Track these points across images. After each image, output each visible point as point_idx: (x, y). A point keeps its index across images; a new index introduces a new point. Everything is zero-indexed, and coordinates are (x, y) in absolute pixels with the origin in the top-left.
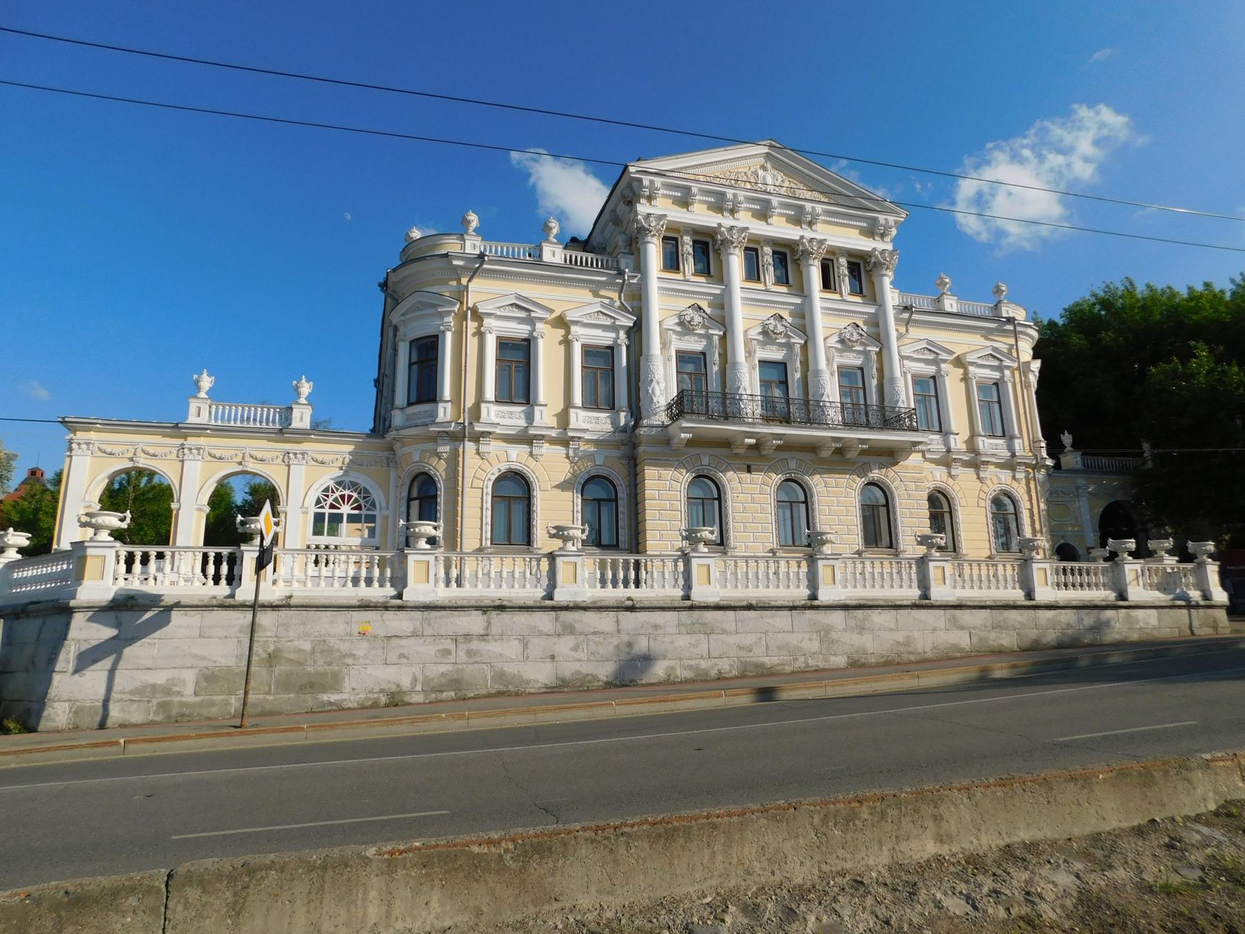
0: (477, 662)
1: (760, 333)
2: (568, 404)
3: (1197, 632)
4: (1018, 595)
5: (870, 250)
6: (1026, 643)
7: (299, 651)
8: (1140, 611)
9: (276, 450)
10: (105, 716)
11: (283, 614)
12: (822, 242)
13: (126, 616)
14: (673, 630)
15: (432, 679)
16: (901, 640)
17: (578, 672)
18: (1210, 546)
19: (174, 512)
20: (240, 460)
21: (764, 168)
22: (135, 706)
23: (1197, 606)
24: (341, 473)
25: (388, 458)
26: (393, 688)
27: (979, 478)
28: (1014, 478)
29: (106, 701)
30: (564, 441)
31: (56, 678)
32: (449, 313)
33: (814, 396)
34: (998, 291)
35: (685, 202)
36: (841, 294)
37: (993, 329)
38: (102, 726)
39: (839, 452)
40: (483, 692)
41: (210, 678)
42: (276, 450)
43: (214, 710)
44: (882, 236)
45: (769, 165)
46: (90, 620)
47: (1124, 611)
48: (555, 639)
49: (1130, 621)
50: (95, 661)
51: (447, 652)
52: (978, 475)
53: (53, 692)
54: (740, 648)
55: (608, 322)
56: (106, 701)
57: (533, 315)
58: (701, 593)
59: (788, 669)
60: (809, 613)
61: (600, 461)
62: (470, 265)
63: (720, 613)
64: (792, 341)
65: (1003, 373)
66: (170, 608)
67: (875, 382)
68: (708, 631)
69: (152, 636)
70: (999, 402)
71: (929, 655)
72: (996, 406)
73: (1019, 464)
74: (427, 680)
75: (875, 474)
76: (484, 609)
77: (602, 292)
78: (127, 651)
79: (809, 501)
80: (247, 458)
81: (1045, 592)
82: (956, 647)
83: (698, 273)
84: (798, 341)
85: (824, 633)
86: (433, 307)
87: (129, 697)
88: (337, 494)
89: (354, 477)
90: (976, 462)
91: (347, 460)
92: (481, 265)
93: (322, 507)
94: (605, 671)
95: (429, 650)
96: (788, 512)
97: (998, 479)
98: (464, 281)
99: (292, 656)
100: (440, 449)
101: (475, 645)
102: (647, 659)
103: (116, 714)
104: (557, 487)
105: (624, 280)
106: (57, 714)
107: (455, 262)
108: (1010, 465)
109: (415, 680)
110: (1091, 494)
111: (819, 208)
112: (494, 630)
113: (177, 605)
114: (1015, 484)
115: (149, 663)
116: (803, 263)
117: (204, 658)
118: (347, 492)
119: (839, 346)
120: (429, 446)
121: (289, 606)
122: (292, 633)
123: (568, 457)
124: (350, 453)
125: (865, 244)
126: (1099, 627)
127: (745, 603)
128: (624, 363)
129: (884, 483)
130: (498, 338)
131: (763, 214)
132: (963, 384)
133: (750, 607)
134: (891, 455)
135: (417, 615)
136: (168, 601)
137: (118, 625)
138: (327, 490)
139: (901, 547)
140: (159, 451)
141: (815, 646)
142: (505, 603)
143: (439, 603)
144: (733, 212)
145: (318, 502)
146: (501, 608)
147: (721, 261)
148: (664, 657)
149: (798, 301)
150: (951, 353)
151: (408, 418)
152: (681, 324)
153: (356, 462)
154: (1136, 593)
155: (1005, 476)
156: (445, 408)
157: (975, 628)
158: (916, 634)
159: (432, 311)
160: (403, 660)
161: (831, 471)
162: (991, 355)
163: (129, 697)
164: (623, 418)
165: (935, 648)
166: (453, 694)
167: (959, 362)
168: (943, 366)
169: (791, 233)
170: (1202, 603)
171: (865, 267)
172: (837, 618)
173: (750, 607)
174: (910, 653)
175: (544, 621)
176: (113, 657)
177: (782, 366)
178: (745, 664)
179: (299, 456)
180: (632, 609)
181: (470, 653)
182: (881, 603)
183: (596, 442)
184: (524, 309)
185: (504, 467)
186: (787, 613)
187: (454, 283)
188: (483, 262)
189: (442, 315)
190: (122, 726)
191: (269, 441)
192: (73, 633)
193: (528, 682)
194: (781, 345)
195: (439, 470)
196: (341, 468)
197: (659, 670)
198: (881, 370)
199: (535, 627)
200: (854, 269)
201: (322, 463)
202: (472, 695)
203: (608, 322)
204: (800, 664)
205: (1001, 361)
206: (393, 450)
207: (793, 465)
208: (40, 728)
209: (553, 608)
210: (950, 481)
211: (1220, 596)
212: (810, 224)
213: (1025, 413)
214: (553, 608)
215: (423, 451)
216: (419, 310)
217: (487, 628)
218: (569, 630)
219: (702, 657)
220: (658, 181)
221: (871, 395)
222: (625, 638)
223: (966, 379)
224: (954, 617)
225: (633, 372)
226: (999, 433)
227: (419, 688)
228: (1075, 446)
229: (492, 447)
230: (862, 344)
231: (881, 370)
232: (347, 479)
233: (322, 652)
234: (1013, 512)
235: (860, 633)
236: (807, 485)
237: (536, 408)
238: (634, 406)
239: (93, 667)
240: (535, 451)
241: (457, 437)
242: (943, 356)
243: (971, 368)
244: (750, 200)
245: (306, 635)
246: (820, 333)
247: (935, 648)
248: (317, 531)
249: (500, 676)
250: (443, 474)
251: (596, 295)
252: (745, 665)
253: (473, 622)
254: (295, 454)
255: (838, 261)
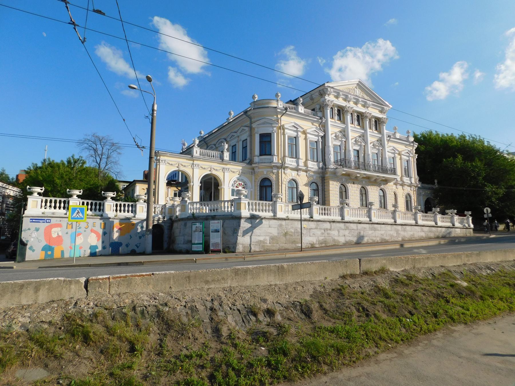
0: (329, 236)
1: (354, 141)
2: (284, 156)
3: (467, 235)
4: (413, 222)
5: (364, 112)
6: (436, 237)
7: (292, 232)
8: (457, 229)
9: (219, 167)
10: (251, 249)
11: (287, 221)
12: (370, 114)
13: (253, 220)
14: (368, 229)
15: (320, 241)
16: (412, 234)
17: (350, 240)
18: (470, 213)
19: (191, 186)
20: (177, 166)
21: (357, 88)
22: (257, 246)
23: (468, 228)
24: (239, 176)
25: (252, 172)
26: (312, 243)
27: (403, 189)
28: (411, 189)
29: (250, 245)
30: (306, 171)
31: (239, 237)
32: (275, 127)
33: (367, 162)
34: (395, 129)
35: (337, 97)
36: (373, 130)
37: (315, 120)
38: (250, 252)
39: (376, 180)
40: (330, 244)
41: (272, 238)
42: (219, 167)
43: (274, 248)
44: (384, 113)
45: (357, 87)
46: (245, 221)
47: (454, 229)
48: (345, 231)
49: (455, 231)
50: (247, 233)
51: (323, 234)
52: (403, 188)
53: (238, 241)
54: (381, 234)
55: (317, 134)
56: (250, 245)
57: (298, 130)
58: (347, 218)
59: (390, 241)
60: (395, 226)
61: (315, 177)
62: (282, 111)
63: (377, 225)
64: (362, 144)
65: (409, 158)
66: (262, 219)
67: (343, 151)
68: (375, 230)
69: (259, 226)
70: (317, 149)
71: (417, 238)
72: (294, 146)
73: (413, 185)
74: (319, 241)
75: (382, 187)
76: (330, 222)
77: (314, 124)
78: (254, 230)
79: (367, 193)
80: (180, 166)
81: (440, 224)
82: (422, 237)
83: (338, 120)
84: (363, 144)
85: (397, 231)
86: (270, 124)
87: (255, 244)
88: (238, 183)
89: (242, 178)
90: (403, 185)
91: (240, 172)
92: (286, 112)
93: (234, 187)
94: (355, 239)
95: (318, 232)
96: (291, 191)
97: (407, 189)
98: (279, 116)
99: (290, 233)
100: (274, 171)
101: (329, 232)
102: (363, 237)
103: (253, 248)
104: (304, 185)
105: (322, 121)
106: (240, 248)
107: (278, 110)
108: (410, 186)
109: (317, 241)
110: (423, 195)
111: (371, 103)
112: (332, 228)
113: (265, 218)
114: (411, 191)
115: (259, 234)
116: (380, 124)
117: (271, 233)
118: (240, 182)
119: (335, 138)
120: (271, 170)
121: (288, 219)
122: (289, 227)
123: (307, 176)
124: (241, 170)
125: (380, 115)
126: (450, 233)
127: (383, 223)
128: (321, 148)
129: (384, 189)
130: (260, 134)
131: (356, 103)
132: (304, 141)
133: (383, 224)
134: (386, 181)
135: (315, 223)
136: (263, 217)
137: (251, 223)
138: (235, 181)
139: (388, 208)
140: (186, 164)
141: (395, 235)
142: (335, 220)
143: (321, 220)
144: (349, 101)
145: (232, 185)
146: (334, 222)
147: (380, 127)
148: (366, 237)
149: (363, 131)
150: (303, 128)
151: (261, 159)
152: (335, 136)
153: (243, 173)
154: (457, 224)
155: (294, 173)
156: (276, 158)
157: (426, 232)
158: (415, 233)
159: (270, 125)
160: (314, 235)
161: (373, 185)
162: (316, 131)
163: (255, 244)
164: (321, 164)
165: (418, 236)
166: (324, 245)
167: (304, 133)
168: (396, 155)
169: (362, 110)
170: (469, 227)
171: (342, 111)
172: (399, 227)
173: (383, 224)
174: (413, 237)
175: (342, 225)
176: (251, 232)
177: (358, 151)
178: (382, 239)
179: (163, 162)
180: (360, 223)
181: (328, 234)
182: (409, 224)
183: (314, 172)
184: (296, 127)
185: (291, 178)
186: (390, 226)
187: (275, 116)
188: (287, 111)
189: (273, 127)
190: (254, 252)
191: (218, 164)
192: (242, 225)
193: (340, 242)
194: (359, 145)
195: (273, 177)
196: (239, 174)
197: (365, 240)
198: (345, 147)
199: (341, 227)
200: (339, 111)
201: (172, 165)
202: (328, 245)
203: (317, 134)
204: (393, 240)
205: (297, 128)
206: (254, 169)
207: (364, 182)
208: (236, 252)
209: (345, 222)
210: (396, 190)
211: (472, 226)
212: (367, 107)
213: (281, 145)
214: (345, 222)
215: (267, 171)
216: (265, 124)
217: (331, 227)
218: (347, 228)
219: (374, 237)
220: (332, 90)
221: (379, 162)
222: (359, 231)
223: (306, 139)
224: (422, 229)
225: (323, 150)
226: (316, 160)
227: (317, 243)
228: (438, 183)
229: (288, 171)
230: (378, 147)
231: (345, 147)
232: (240, 178)
233: (296, 232)
234: (296, 187)
235: (404, 232)
236: (347, 187)
237: (300, 160)
238: (324, 161)
239: (247, 235)
240: (299, 174)
241: (278, 168)
242: (397, 152)
243: (402, 156)
244: (362, 101)
245: (292, 227)
246: (350, 138)
247: (418, 236)
248: (233, 195)
249: (334, 240)
250: (275, 179)
251: (313, 124)
252: (382, 239)
253: (327, 225)
254: (226, 169)
255: (334, 108)
